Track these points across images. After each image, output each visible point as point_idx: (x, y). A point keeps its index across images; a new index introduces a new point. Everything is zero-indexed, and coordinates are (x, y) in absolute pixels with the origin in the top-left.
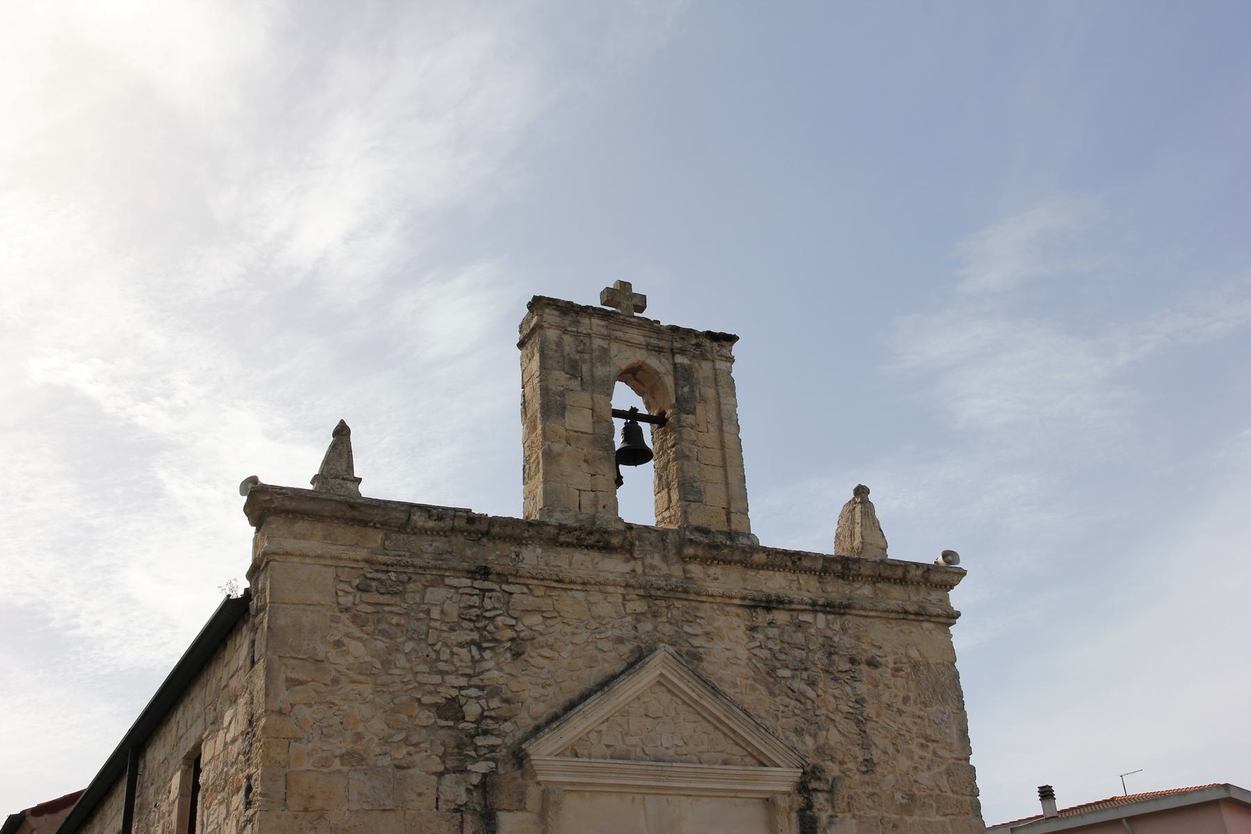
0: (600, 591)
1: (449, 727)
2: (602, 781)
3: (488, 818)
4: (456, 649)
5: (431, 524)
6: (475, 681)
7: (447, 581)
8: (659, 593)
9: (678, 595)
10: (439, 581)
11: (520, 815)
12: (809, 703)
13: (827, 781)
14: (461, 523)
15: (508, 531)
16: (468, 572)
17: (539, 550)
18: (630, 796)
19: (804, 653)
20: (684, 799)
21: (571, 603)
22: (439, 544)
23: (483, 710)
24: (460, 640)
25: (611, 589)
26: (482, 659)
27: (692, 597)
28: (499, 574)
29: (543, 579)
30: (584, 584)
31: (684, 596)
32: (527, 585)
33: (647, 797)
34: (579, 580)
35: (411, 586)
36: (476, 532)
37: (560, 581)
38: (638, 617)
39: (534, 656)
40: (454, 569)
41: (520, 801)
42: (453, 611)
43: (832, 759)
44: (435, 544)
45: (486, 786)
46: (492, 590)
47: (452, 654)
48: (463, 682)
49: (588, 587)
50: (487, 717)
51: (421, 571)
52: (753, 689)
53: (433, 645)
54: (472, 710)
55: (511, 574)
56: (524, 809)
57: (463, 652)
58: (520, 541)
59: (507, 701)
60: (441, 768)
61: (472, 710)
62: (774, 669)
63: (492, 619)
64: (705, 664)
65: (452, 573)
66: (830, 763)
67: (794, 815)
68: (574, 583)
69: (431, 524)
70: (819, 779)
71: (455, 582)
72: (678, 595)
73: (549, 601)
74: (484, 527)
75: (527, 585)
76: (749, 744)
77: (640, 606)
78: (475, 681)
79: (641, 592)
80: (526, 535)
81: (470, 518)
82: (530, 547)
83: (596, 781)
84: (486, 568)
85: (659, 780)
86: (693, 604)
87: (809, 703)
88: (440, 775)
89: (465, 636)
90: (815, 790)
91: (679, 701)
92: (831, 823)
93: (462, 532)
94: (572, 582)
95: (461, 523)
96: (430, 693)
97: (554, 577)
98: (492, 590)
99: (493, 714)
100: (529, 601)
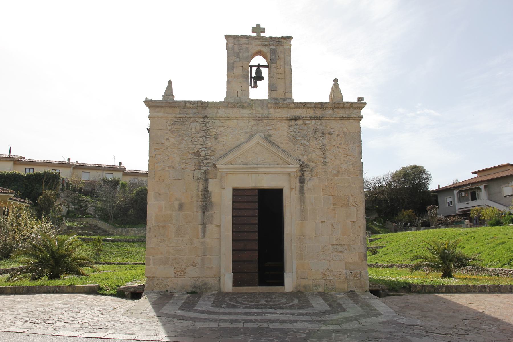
5: (191, 106)
6: (204, 146)
10: (194, 121)
11: (215, 180)
12: (306, 147)
14: (200, 105)
25: (244, 119)
26: (206, 140)
35: (187, 123)
38: (253, 126)
42: (198, 129)
43: (313, 162)
45: (206, 173)
48: (201, 147)
52: (288, 143)
54: (203, 154)
56: (216, 178)
59: (212, 151)
61: (203, 154)
62: (295, 138)
64: (272, 138)
67: (298, 178)
69: (191, 106)
77: (253, 123)
78: (204, 146)
81: (202, 103)
87: (306, 147)
88: (194, 170)
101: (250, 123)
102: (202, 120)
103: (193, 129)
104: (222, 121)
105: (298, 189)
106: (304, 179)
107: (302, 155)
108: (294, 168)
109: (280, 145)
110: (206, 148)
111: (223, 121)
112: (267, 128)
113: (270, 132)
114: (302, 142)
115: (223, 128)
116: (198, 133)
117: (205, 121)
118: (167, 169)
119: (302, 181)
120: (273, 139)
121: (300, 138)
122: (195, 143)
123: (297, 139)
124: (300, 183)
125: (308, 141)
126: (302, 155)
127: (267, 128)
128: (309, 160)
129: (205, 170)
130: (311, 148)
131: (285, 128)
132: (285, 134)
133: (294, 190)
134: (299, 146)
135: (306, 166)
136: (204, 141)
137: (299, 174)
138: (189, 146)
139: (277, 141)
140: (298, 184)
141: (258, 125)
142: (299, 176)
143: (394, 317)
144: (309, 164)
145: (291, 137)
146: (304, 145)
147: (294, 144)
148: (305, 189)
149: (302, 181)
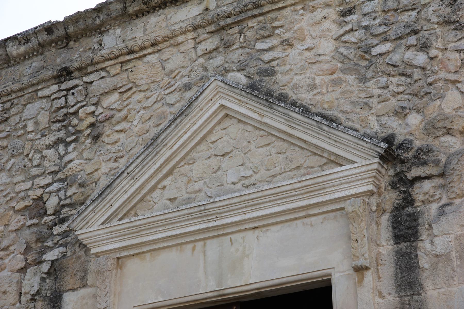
0: (172, 45)
1: (34, 225)
2: (151, 238)
3: (56, 300)
4: (45, 152)
5: (22, 49)
6: (60, 176)
7: (40, 94)
8: (229, 21)
9: (250, 13)
10: (35, 97)
11: (82, 292)
12: (417, 74)
13: (437, 162)
14: (44, 37)
15: (81, 25)
16: (54, 77)
17: (118, 31)
18: (190, 246)
19: (414, 13)
20: (250, 233)
21: (144, 71)
22: (37, 63)
23: (60, 199)
24: (47, 142)
25: (180, 39)
26: (67, 153)
27: (266, 9)
28: (80, 69)
29: (117, 57)
30: (153, 45)
31: (255, 12)
32: (103, 69)
33: (208, 242)
34: (147, 43)
35: (14, 110)
36: (60, 39)
37: (131, 52)
38: (209, 54)
39: (109, 134)
40: (44, 81)
41: (84, 278)
42: (44, 119)
43: (449, 131)
44: (34, 65)
45: (55, 270)
46: (76, 86)
47: (43, 157)
48: (48, 179)
49: (160, 46)
50: (63, 206)
51: (20, 94)
52: (337, 83)
53: (28, 155)
54: (52, 203)
55: (89, 65)
56: (85, 286)
57: (50, 153)
58: (100, 30)
59: (82, 185)
60: (22, 265)
61: (52, 203)
62: (368, 50)
63: (76, 113)
64: (278, 77)
65: (43, 85)
66: (447, 138)
67: (385, 219)
68: (145, 48)
69: (22, 49)
70: (425, 163)
71: (47, 92)
72: (250, 13)
73: (124, 75)
74: (61, 32)
75: (103, 69)
76: (323, 150)
77: (211, 43)
78: (60, 176)
79: (212, 28)
80: (98, 21)
81: (49, 28)
82: (111, 31)
83: (145, 239)
84: (66, 68)
85: (209, 221)
86: (270, 15)
87: (417, 74)
88: (23, 270)
89: (52, 138)
90: (418, 179)
91: (250, 128)
92: (441, 213)
93: (50, 44)
94: (142, 48)
95: (44, 37)
96: (23, 199)
97: (125, 51)
98: (76, 86)
99: (68, 201)
100: (109, 83)
101: (201, 48)
102: (55, 87)
103: (30, 127)
104: (114, 71)
105: (388, 270)
106: (414, 218)
107: (401, 113)
108: (359, 173)
109: (305, 97)
110: (62, 180)
111: (117, 69)
112: (260, 46)
113: (267, 57)
114: (396, 58)
115: (116, 96)
116: (43, 136)
117: (63, 86)
118: (220, 164)
119: (406, 228)
120: (281, 82)
121: (388, 46)
122: (34, 171)
123: (376, 51)
124: (398, 237)
125: (424, 47)
126: (401, 113)
127: (260, 46)
128: (431, 128)
129: (53, 262)
130: (442, 75)
131: (327, 24)
132: (327, 47)
133: (369, 277)
134: (383, 80)
135: (422, 156)
136: (61, 157)
137: (391, 198)
138: (17, 189)
139: (296, 87)
140: (387, 248)
141: (227, 47)
142: (389, 207)
143: (235, 19)
144: (435, 144)
145: (350, 53)
146: (403, 70)
147: (363, 79)
148: (424, 262)
149: (406, 228)
